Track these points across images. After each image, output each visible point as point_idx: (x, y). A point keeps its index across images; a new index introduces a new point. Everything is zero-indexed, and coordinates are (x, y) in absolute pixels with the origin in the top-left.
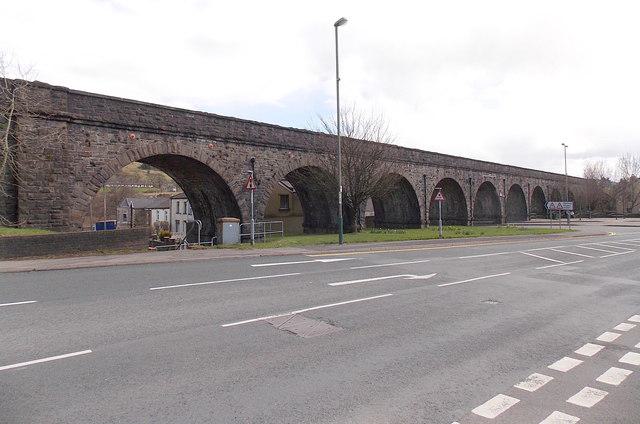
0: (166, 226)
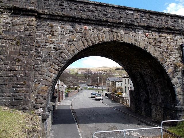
0: (121, 89)
